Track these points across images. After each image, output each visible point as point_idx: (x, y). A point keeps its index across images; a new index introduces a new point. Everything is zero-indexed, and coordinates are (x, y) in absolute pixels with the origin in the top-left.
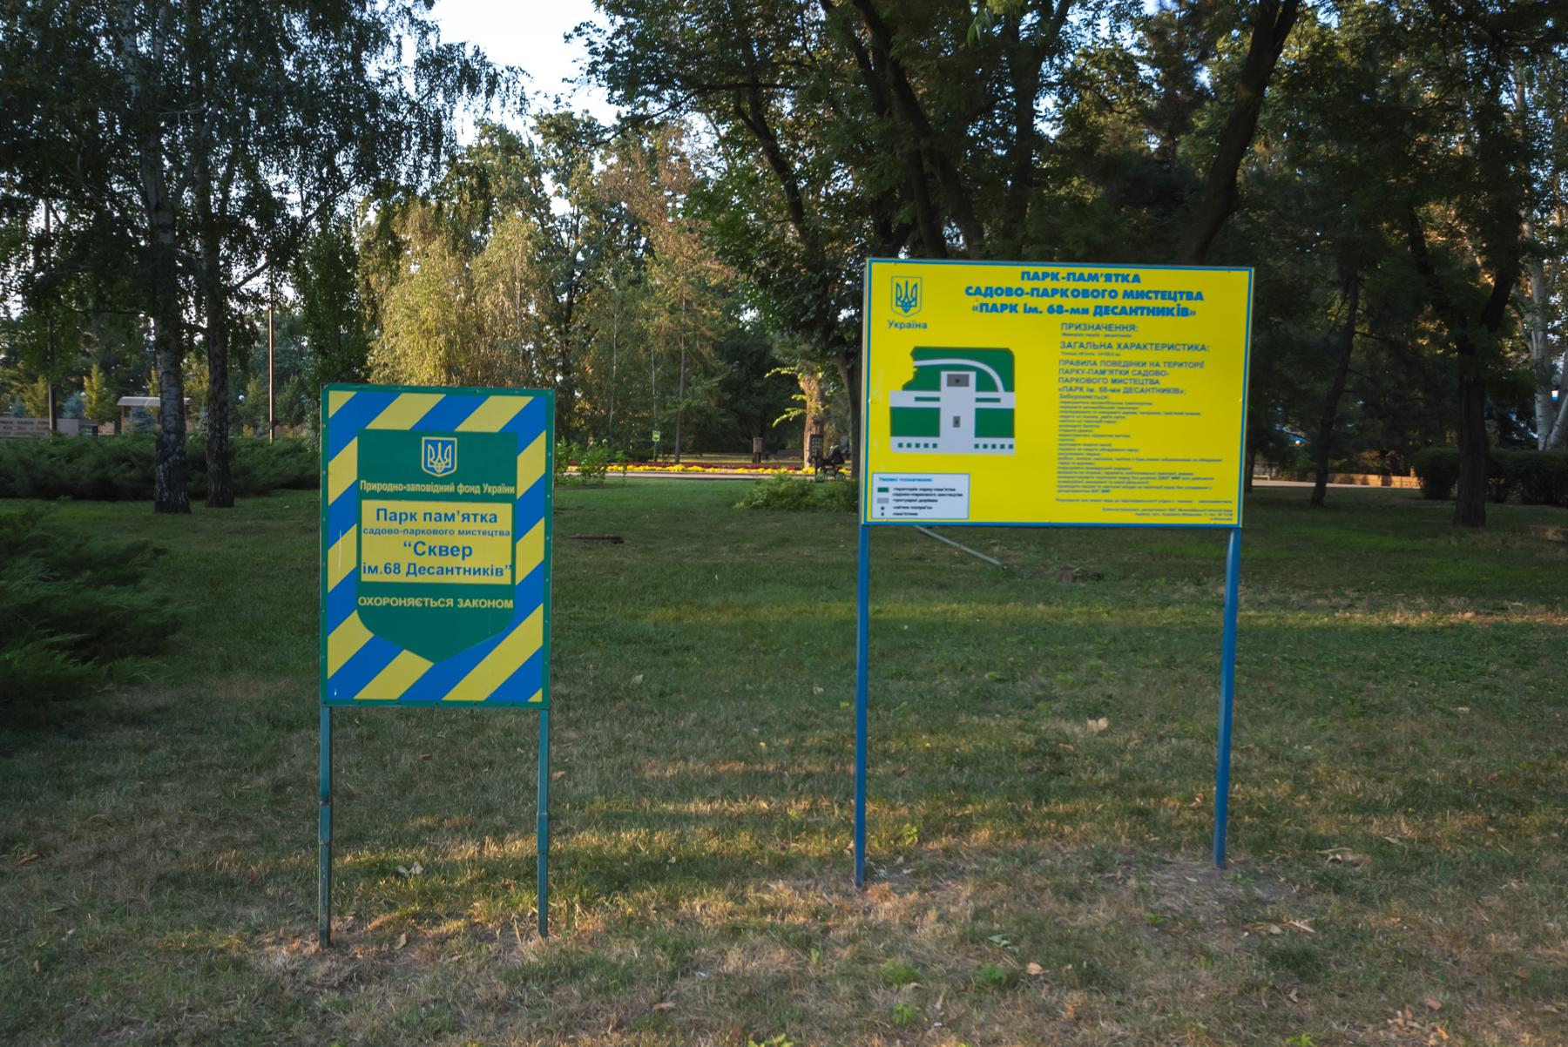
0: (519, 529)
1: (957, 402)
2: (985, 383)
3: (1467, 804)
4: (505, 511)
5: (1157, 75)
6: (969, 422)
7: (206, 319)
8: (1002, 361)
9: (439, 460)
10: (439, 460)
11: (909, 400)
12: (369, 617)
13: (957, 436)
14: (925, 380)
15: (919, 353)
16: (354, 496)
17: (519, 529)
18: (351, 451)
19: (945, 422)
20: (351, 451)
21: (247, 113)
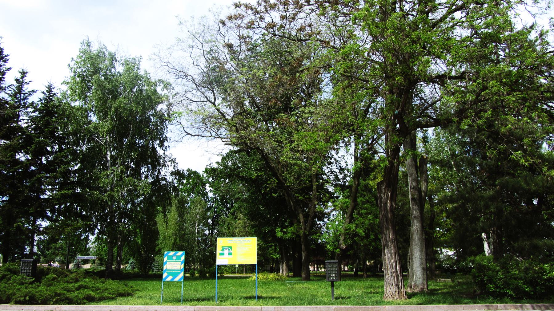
0: (181, 264)
1: (226, 252)
2: (229, 250)
3: (133, 291)
4: (180, 263)
5: (369, 180)
6: (228, 254)
7: (400, 173)
8: (231, 248)
9: (174, 258)
10: (174, 258)
11: (221, 252)
12: (167, 273)
13: (226, 255)
14: (223, 250)
15: (222, 247)
16: (166, 262)
17: (181, 264)
18: (166, 257)
19: (225, 254)
20: (166, 257)
21: (77, 208)
